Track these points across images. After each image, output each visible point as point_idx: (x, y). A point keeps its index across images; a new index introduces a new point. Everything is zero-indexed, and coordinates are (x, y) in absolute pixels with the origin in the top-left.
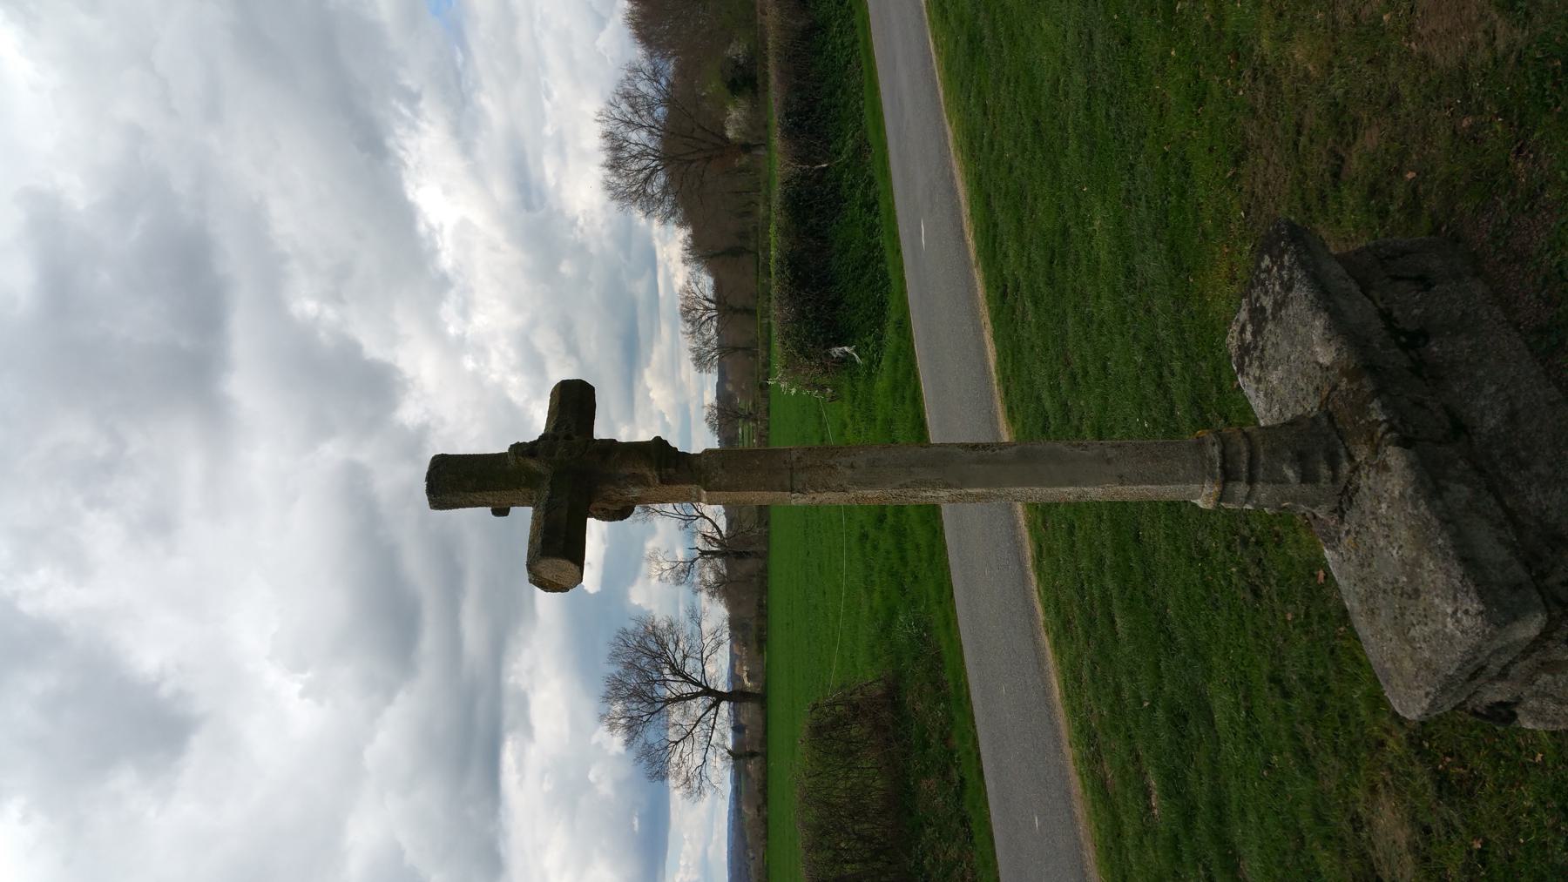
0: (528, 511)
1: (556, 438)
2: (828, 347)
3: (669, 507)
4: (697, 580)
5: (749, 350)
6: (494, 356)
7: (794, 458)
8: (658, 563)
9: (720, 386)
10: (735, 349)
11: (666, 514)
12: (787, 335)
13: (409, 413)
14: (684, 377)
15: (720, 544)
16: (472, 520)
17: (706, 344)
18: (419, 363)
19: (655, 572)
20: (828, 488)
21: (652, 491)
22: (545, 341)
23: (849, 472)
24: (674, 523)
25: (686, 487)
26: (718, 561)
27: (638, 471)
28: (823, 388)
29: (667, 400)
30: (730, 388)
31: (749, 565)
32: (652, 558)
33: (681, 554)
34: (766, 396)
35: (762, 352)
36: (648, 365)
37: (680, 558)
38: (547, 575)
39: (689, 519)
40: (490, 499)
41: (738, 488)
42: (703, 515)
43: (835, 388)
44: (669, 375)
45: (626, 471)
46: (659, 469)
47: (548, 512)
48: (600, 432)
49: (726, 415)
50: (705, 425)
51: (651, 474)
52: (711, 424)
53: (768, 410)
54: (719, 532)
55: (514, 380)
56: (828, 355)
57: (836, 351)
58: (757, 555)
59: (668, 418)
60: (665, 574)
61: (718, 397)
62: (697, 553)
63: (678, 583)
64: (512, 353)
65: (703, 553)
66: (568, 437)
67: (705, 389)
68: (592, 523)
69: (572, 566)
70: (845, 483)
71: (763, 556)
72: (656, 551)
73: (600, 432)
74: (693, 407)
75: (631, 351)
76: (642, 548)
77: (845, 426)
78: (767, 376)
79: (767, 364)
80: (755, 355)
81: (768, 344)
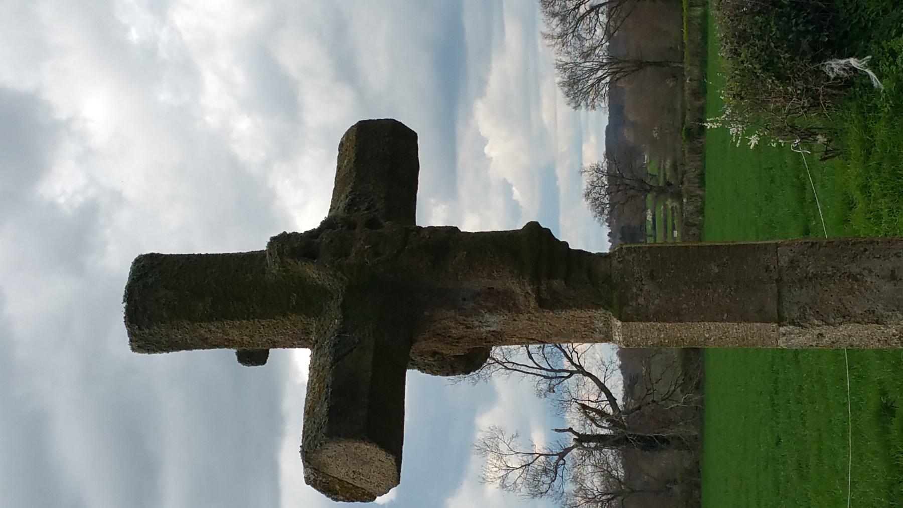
0: (300, 359)
1: (352, 226)
2: (819, 58)
3: (518, 353)
4: (570, 488)
5: (665, 66)
6: (210, 80)
7: (784, 261)
8: (500, 456)
9: (611, 132)
10: (640, 65)
11: (515, 367)
12: (742, 37)
13: (64, 184)
14: (546, 117)
15: (614, 423)
16: (199, 370)
17: (586, 56)
18: (92, 105)
19: (493, 472)
20: (847, 317)
21: (523, 322)
22: (299, 55)
23: (887, 288)
24: (528, 384)
25: (584, 314)
26: (610, 454)
27: (498, 285)
28: (808, 135)
29: (521, 158)
30: (628, 135)
31: (666, 461)
32: (489, 447)
33: (540, 441)
34: (700, 152)
35: (690, 70)
36: (481, 94)
37: (539, 448)
38: (338, 471)
39: (555, 376)
40: (235, 334)
41: (678, 316)
42: (581, 370)
43: (833, 134)
44: (521, 113)
45: (478, 283)
46: (529, 278)
47: (337, 358)
48: (432, 212)
49: (623, 186)
50: (585, 205)
51: (521, 289)
52: (596, 203)
53: (702, 176)
54: (611, 400)
55: (244, 125)
56: (818, 73)
57: (835, 66)
58: (681, 443)
59: (517, 194)
60: (514, 476)
61: (609, 154)
62: (571, 439)
63: (537, 493)
64: (240, 76)
65: (582, 439)
66: (372, 224)
67: (584, 138)
68: (414, 378)
69: (382, 455)
70: (880, 309)
71: (693, 445)
72: (496, 433)
73: (432, 212)
74: (562, 173)
75: (452, 66)
76: (471, 427)
77: (850, 205)
78: (701, 114)
79: (700, 92)
80: (677, 75)
81: (702, 56)
